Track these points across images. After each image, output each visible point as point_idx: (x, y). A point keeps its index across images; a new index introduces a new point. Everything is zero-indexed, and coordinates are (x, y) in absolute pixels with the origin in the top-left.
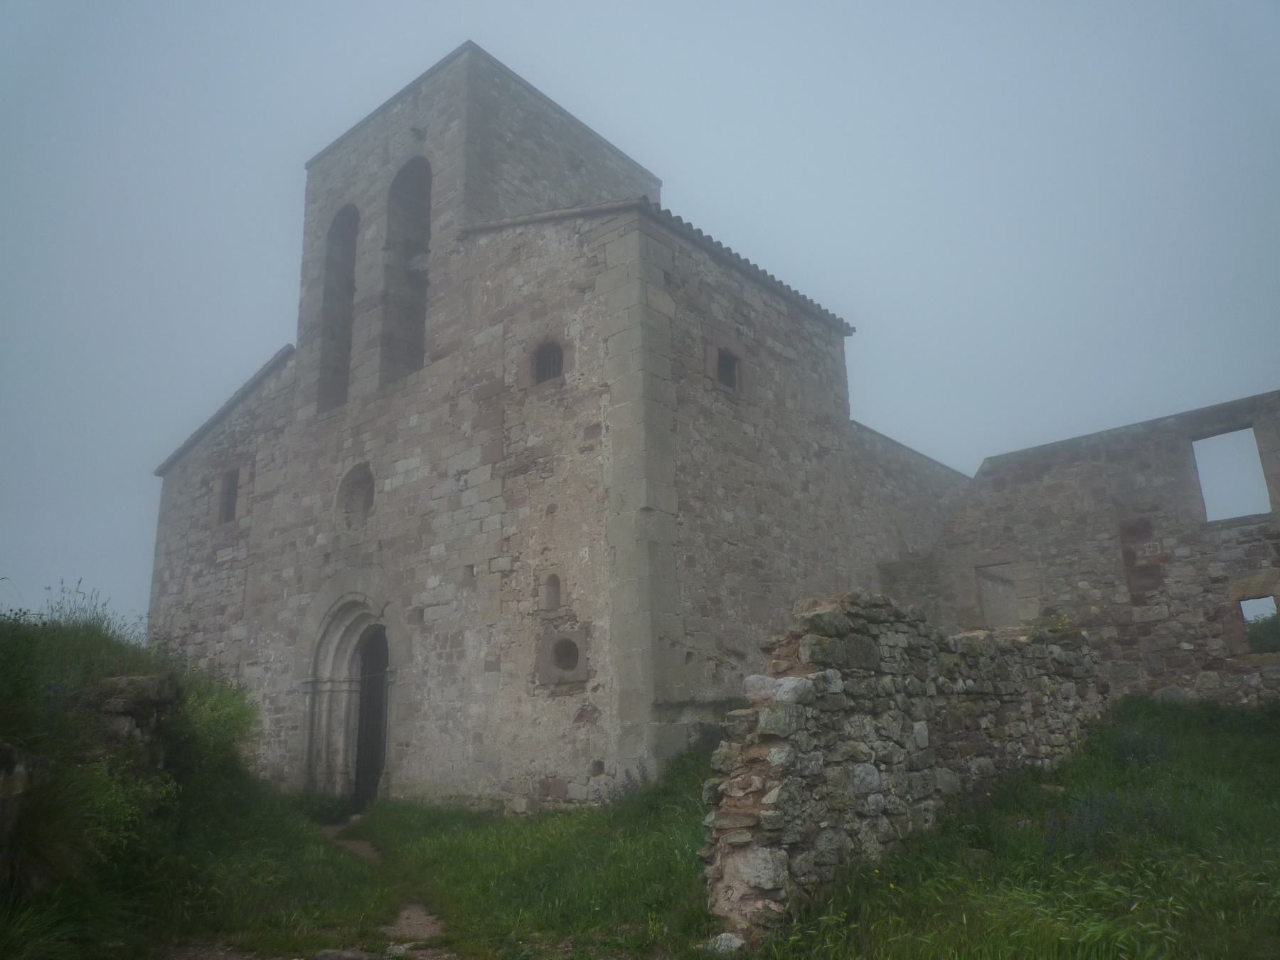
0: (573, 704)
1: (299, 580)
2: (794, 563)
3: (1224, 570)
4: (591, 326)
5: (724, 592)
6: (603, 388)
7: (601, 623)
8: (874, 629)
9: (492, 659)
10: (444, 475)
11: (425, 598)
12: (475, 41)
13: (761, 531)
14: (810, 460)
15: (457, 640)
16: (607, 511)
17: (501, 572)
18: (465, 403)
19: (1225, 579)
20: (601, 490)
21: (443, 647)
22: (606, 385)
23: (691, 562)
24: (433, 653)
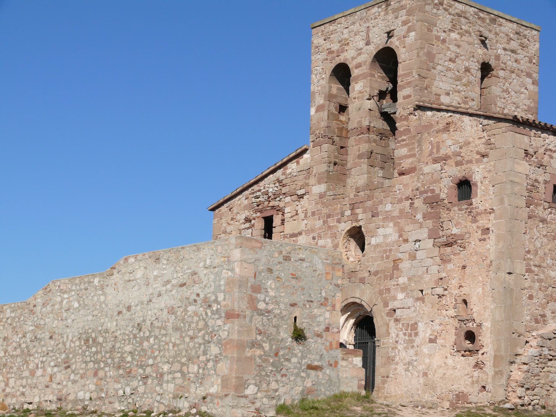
0: (472, 360)
9: (433, 337)
10: (406, 241)
15: (414, 327)
18: (418, 203)
21: (407, 330)
22: (493, 209)
23: (531, 297)
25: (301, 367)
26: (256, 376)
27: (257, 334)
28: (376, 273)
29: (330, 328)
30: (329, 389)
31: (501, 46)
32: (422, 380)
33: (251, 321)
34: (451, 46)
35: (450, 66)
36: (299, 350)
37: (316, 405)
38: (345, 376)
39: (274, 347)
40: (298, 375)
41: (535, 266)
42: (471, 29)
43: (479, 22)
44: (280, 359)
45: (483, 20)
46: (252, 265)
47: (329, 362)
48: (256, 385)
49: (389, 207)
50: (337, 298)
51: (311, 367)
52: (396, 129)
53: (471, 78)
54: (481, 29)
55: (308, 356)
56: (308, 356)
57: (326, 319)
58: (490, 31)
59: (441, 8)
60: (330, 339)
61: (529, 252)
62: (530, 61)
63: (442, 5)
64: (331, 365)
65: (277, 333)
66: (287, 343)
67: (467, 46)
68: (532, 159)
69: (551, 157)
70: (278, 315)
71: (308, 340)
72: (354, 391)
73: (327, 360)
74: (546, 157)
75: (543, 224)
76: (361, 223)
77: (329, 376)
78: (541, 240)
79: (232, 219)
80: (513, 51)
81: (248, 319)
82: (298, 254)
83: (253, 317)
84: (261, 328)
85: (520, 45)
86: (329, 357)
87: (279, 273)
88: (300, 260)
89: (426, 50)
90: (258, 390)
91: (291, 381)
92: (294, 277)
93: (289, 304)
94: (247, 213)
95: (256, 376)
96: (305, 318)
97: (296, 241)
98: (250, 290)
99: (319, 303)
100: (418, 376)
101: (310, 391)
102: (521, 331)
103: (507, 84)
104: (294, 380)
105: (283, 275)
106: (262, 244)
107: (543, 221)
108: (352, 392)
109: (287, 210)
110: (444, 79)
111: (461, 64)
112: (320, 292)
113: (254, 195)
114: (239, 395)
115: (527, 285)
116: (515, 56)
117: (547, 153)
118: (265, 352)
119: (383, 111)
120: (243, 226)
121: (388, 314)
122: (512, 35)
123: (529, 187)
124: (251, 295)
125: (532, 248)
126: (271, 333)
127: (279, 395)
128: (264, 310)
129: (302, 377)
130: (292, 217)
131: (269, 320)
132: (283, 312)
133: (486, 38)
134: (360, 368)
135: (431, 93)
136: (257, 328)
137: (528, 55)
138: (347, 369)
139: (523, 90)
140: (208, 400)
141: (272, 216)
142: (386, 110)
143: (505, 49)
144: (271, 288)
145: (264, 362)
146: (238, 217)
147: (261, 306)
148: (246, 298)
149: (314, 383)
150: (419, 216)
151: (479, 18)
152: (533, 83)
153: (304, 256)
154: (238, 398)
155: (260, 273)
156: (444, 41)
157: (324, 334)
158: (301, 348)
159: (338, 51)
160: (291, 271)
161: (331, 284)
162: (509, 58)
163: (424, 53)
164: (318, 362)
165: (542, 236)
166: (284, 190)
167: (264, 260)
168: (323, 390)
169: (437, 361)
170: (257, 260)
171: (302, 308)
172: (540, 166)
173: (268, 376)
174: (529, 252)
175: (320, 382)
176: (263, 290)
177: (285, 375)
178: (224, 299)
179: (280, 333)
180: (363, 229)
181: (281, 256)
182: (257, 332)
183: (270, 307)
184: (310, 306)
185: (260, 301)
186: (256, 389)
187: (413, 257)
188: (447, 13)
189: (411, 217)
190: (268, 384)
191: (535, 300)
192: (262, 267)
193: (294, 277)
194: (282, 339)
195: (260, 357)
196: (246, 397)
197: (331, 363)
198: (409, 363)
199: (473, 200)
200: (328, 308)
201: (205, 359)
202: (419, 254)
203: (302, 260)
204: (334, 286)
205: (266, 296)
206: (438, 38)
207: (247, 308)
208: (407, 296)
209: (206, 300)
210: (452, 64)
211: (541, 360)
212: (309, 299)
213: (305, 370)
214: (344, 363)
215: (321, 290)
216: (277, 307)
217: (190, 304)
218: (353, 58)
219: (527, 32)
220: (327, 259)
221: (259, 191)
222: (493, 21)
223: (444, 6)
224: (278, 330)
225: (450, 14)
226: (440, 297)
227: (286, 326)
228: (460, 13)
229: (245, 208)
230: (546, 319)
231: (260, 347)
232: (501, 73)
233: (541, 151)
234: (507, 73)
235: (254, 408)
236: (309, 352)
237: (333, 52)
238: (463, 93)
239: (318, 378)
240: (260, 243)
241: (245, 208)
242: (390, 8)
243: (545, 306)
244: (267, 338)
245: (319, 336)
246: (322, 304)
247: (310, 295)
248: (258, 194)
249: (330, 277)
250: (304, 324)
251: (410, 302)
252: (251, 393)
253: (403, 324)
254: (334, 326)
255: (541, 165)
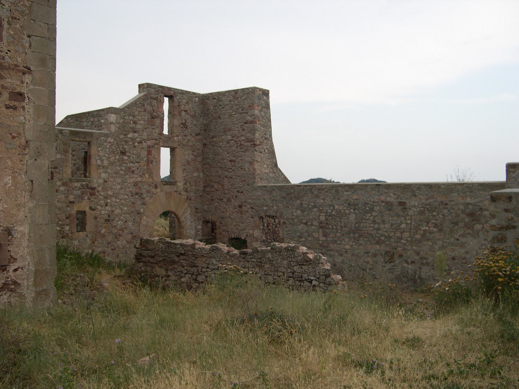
3: (74, 199)
4: (18, 18)
6: (25, 69)
7: (22, 229)
12: (270, 92)
16: (28, 156)
19: (74, 202)
20: (23, 141)
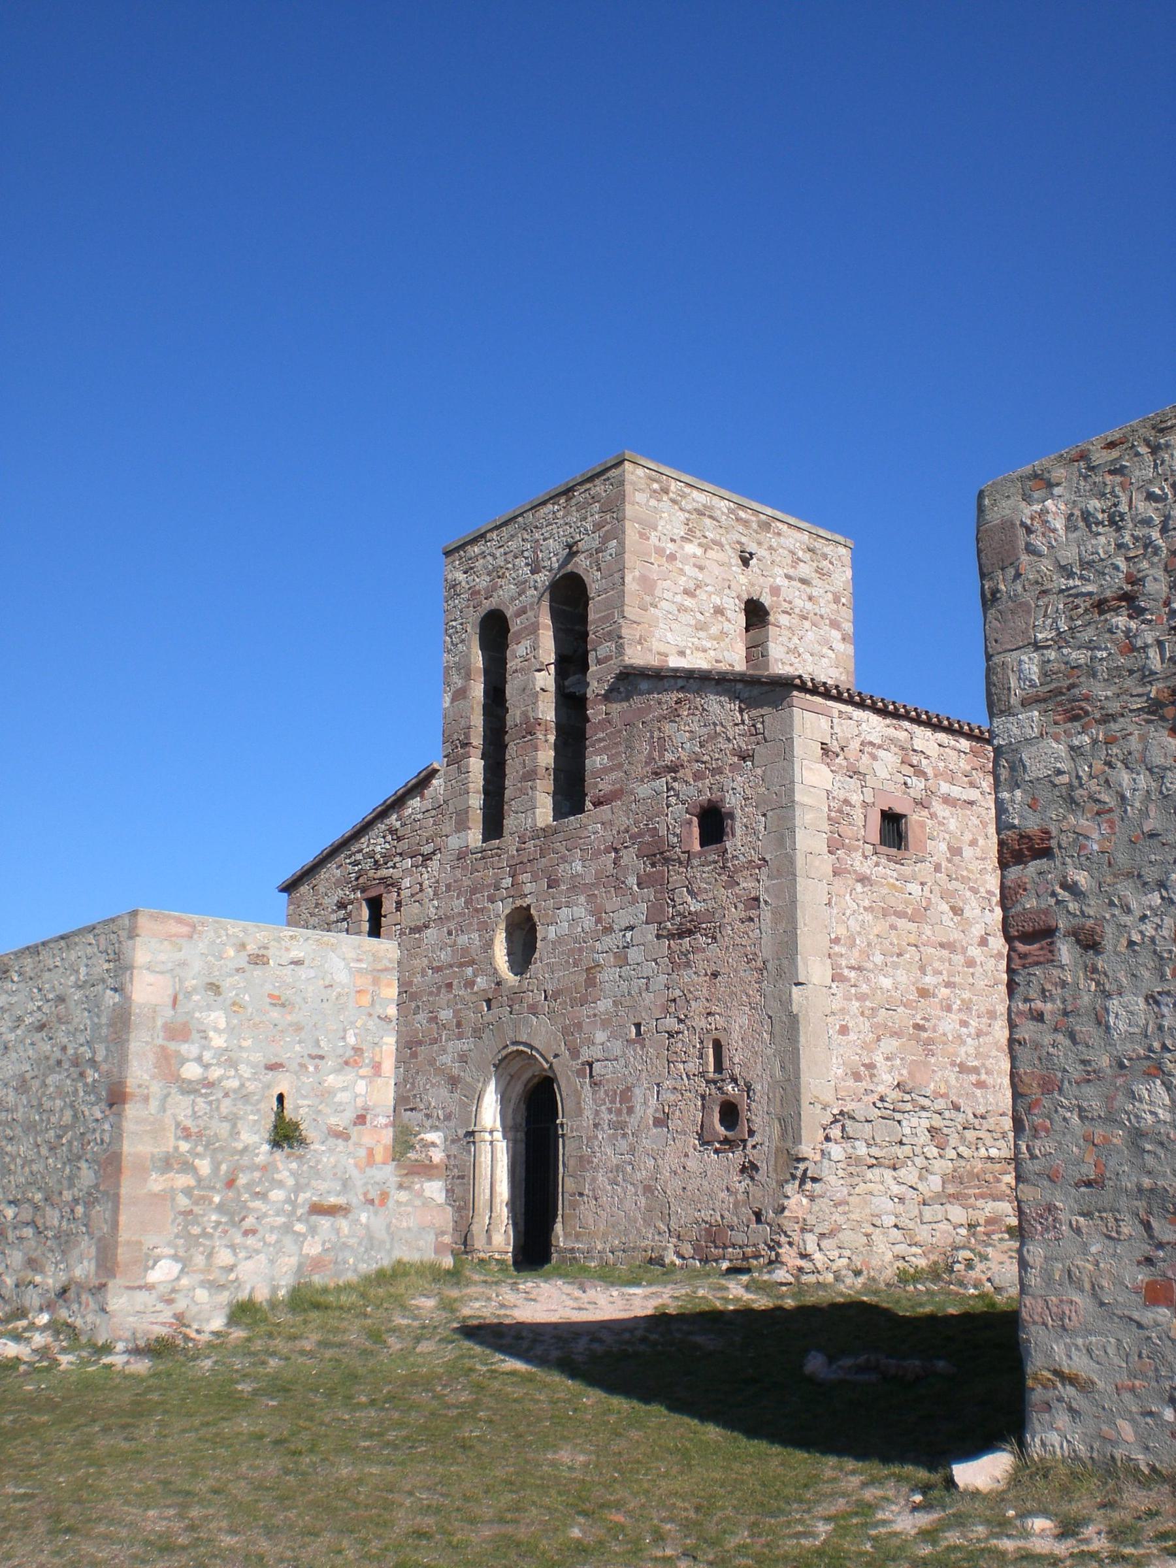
0: (736, 1158)
1: (459, 1025)
2: (964, 1024)
5: (879, 1059)
8: (898, 1116)
9: (660, 1115)
10: (608, 930)
11: (595, 1052)
13: (924, 993)
14: (991, 911)
15: (626, 1095)
17: (667, 1032)
18: (629, 856)
21: (613, 1102)
22: (764, 859)
23: (844, 1030)
24: (603, 1108)
25: (293, 1212)
26: (177, 1236)
27: (178, 1138)
28: (557, 994)
29: (368, 1117)
30: (366, 1257)
31: (781, 572)
32: (643, 1201)
33: (163, 1108)
34: (687, 568)
35: (686, 603)
36: (290, 1171)
37: (321, 1299)
38: (405, 1224)
39: (224, 1167)
40: (287, 1229)
41: (852, 968)
42: (723, 540)
43: (741, 528)
44: (239, 1195)
45: (746, 523)
46: (168, 975)
47: (365, 1194)
48: (175, 1258)
49: (578, 867)
50: (384, 1047)
51: (318, 1209)
52: (588, 721)
53: (727, 626)
54: (744, 540)
55: (314, 1183)
56: (314, 1183)
57: (356, 1096)
58: (759, 544)
59: (665, 498)
60: (367, 1140)
61: (836, 941)
62: (836, 600)
63: (667, 493)
64: (372, 1202)
65: (231, 1135)
66: (257, 1155)
67: (717, 570)
68: (837, 761)
69: (874, 757)
70: (235, 1091)
71: (312, 1147)
72: (425, 1259)
73: (360, 1191)
74: (865, 758)
75: (864, 886)
76: (528, 901)
77: (367, 1227)
78: (860, 918)
79: (317, 905)
80: (804, 581)
81: (154, 1105)
82: (287, 949)
83: (169, 1099)
84: (188, 1123)
85: (816, 571)
86: (366, 1184)
87: (237, 995)
88: (292, 963)
89: (637, 573)
90: (182, 1271)
91: (270, 1245)
92: (278, 1002)
93: (262, 1064)
94: (338, 894)
95: (177, 1236)
96: (305, 1097)
97: (420, 940)
98: (161, 1034)
99: (340, 1061)
100: (636, 1194)
101: (317, 1264)
102: (827, 1099)
103: (795, 640)
104: (277, 1242)
105: (247, 997)
106: (194, 927)
107: (863, 879)
108: (421, 1262)
109: (406, 883)
110: (675, 626)
111: (709, 599)
112: (342, 1034)
113: (352, 859)
114: (131, 1284)
115: (835, 1006)
116: (808, 590)
117: (866, 749)
118: (199, 1180)
119: (567, 691)
120: (334, 917)
121: (580, 1073)
122: (800, 554)
123: (833, 814)
124: (163, 1048)
125: (841, 931)
126: (216, 1134)
127: (237, 1279)
128: (198, 1082)
129: (298, 1234)
130: (412, 895)
131: (210, 1103)
132: (248, 1084)
133: (751, 554)
134: (439, 1205)
135: (651, 650)
136: (178, 1125)
137: (832, 589)
138: (410, 1209)
139: (825, 650)
140: (71, 1294)
141: (381, 895)
142: (572, 690)
143: (788, 577)
144: (216, 1030)
145: (198, 1204)
146: (326, 901)
147: (192, 1071)
148: (151, 1056)
149: (328, 1245)
150: (632, 881)
151: (738, 519)
152: (844, 639)
153: (302, 954)
154: (130, 1292)
155: (188, 995)
156: (672, 557)
157: (354, 1132)
158: (294, 1165)
159: (486, 589)
160: (268, 988)
161: (370, 1015)
162: (797, 593)
163: (633, 579)
164: (338, 1195)
165: (862, 910)
166: (403, 846)
167: (197, 965)
168: (351, 1261)
169: (671, 1160)
170: (183, 964)
171: (296, 1073)
172: (854, 773)
173: (210, 1236)
174: (836, 941)
175: (344, 1244)
176: (195, 1036)
177: (254, 1232)
178: (105, 1060)
179: (238, 1133)
180: (532, 911)
181: (244, 954)
182: (179, 1133)
183: (215, 1073)
184: (316, 1067)
185: (188, 1060)
186: (177, 1267)
187: (621, 959)
188: (676, 507)
189: (619, 886)
190: (210, 1256)
191: (852, 1036)
192: (194, 982)
193: (278, 1002)
194: (246, 1149)
195: (188, 1192)
196: (149, 1288)
197: (370, 1197)
198: (618, 1168)
199: (728, 844)
200: (362, 1072)
201: (70, 1198)
202: (634, 955)
203: (297, 963)
204: (377, 1020)
205: (204, 1048)
206: (660, 551)
207: (153, 1077)
208: (613, 1036)
209: (75, 1063)
210: (689, 599)
211: (851, 1169)
212: (315, 1052)
213: (304, 1218)
214: (403, 1196)
215: (345, 1030)
216: (232, 1073)
217: (51, 1070)
218: (513, 599)
219: (829, 549)
220: (359, 960)
221: (360, 851)
222: (765, 526)
223: (671, 495)
224: (234, 1126)
225: (681, 509)
226: (671, 1035)
227: (256, 1118)
228: (701, 508)
229: (338, 884)
230: (875, 1071)
231: (187, 1167)
232: (784, 620)
233: (855, 745)
234: (795, 620)
235: (170, 1314)
236: (316, 1173)
237: (478, 592)
238: (712, 653)
239: (338, 1233)
240: (188, 924)
241: (338, 884)
242: (573, 502)
243: (873, 1046)
244: (206, 1147)
245: (342, 1135)
246: (347, 1063)
247: (317, 1042)
248: (359, 856)
249: (366, 1000)
250: (301, 1111)
251: (617, 1047)
252: (163, 1278)
253: (606, 1092)
254: (378, 1110)
255: (855, 773)
